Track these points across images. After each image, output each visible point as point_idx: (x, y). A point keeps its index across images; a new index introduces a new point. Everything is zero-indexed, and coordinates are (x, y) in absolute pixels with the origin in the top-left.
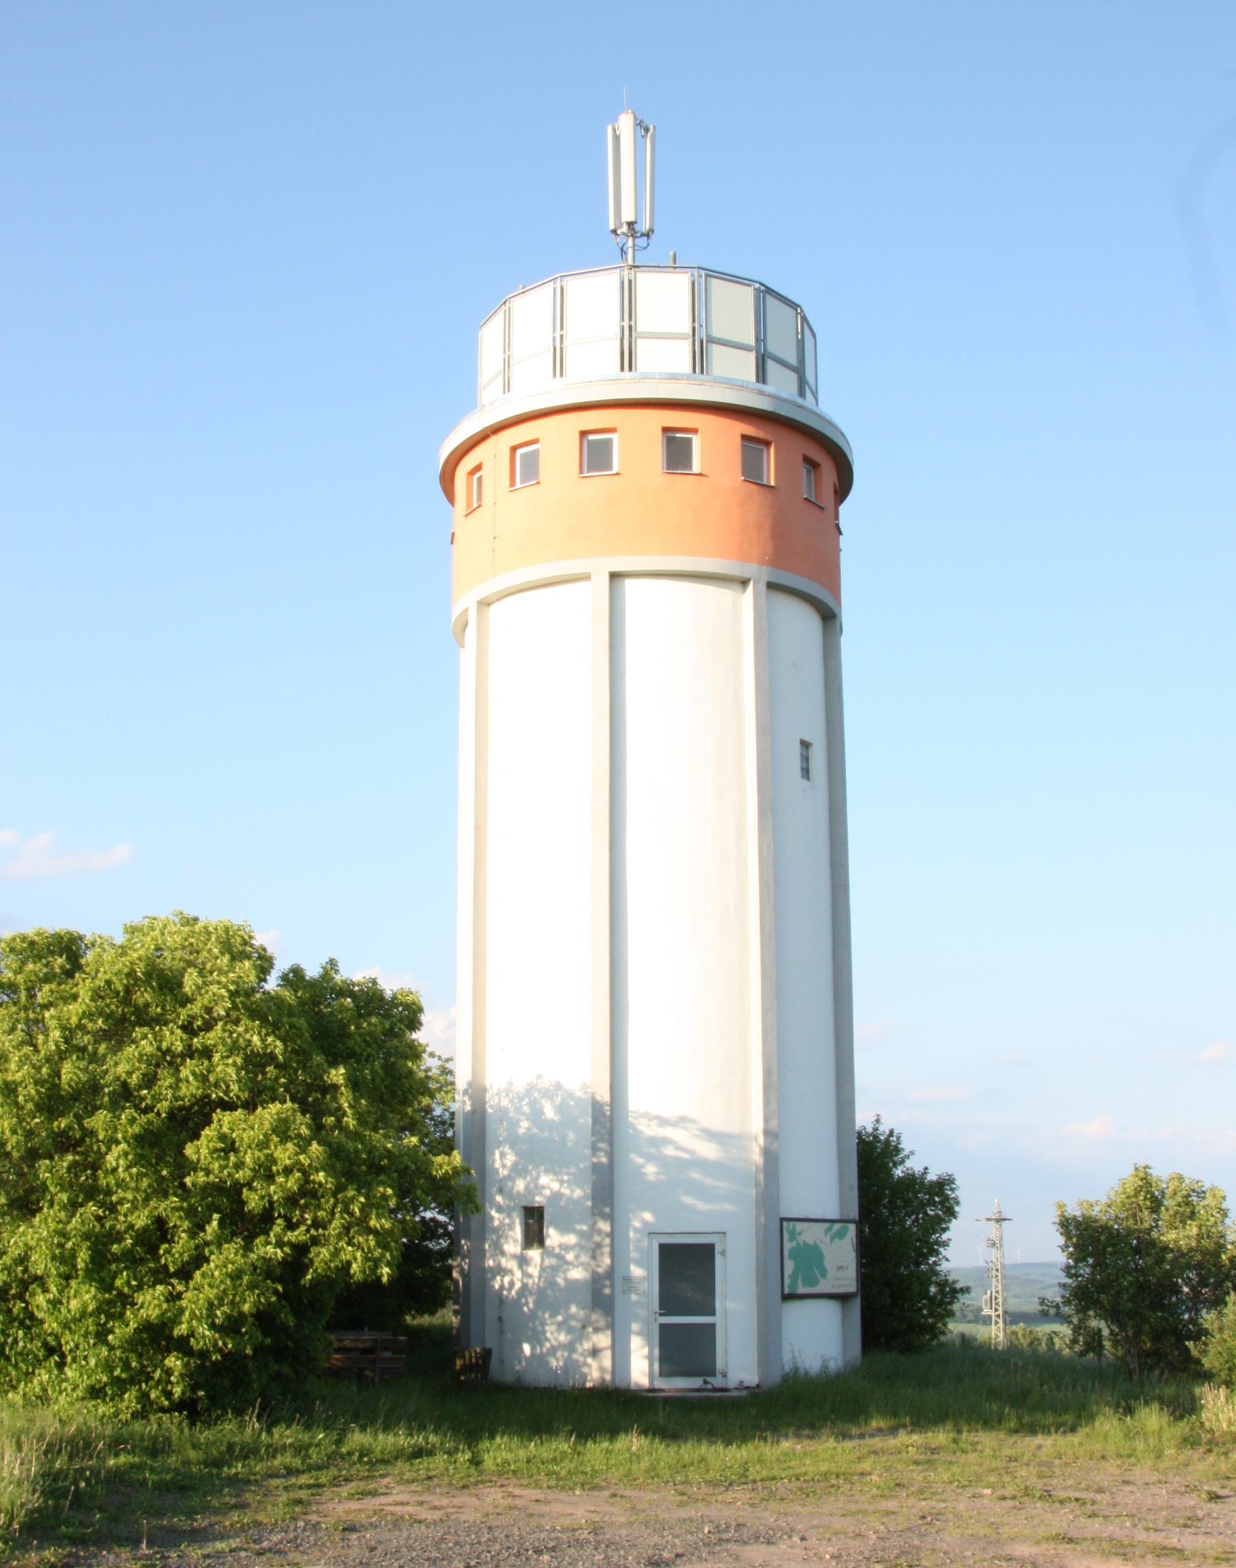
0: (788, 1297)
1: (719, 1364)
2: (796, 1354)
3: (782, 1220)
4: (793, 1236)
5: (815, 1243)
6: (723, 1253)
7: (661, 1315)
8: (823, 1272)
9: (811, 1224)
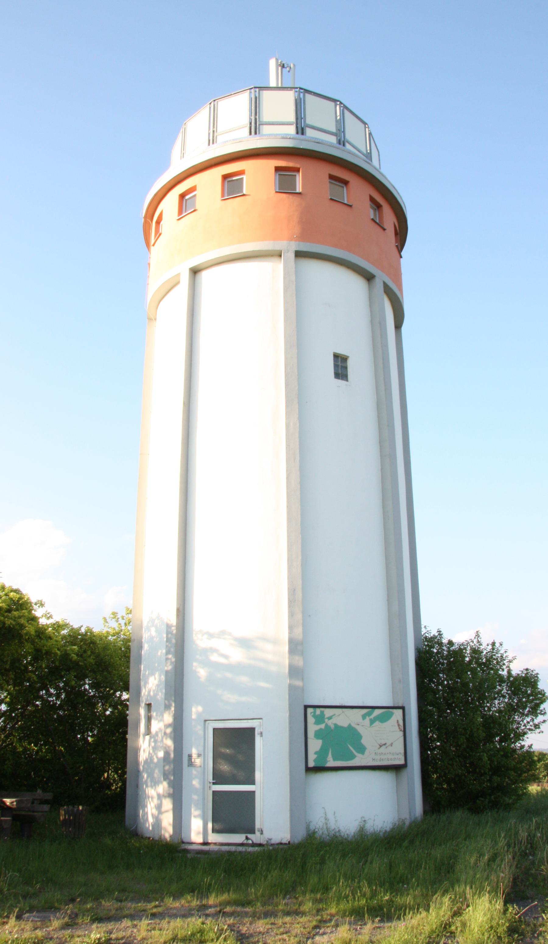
0: (319, 769)
1: (258, 825)
2: (330, 816)
3: (306, 707)
4: (320, 720)
5: (350, 725)
6: (261, 734)
7: (214, 784)
8: (362, 749)
9: (344, 710)
